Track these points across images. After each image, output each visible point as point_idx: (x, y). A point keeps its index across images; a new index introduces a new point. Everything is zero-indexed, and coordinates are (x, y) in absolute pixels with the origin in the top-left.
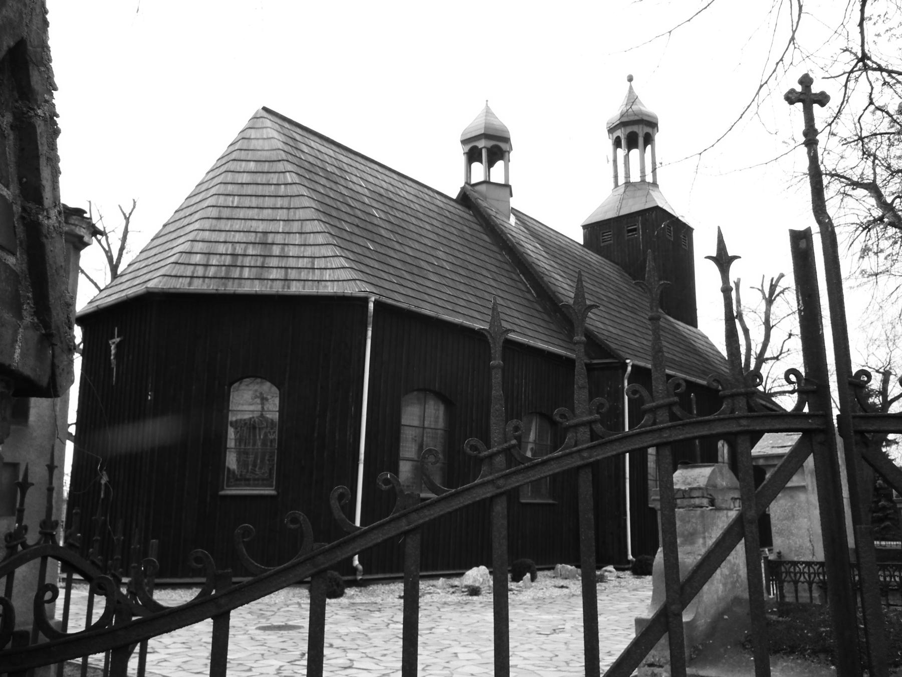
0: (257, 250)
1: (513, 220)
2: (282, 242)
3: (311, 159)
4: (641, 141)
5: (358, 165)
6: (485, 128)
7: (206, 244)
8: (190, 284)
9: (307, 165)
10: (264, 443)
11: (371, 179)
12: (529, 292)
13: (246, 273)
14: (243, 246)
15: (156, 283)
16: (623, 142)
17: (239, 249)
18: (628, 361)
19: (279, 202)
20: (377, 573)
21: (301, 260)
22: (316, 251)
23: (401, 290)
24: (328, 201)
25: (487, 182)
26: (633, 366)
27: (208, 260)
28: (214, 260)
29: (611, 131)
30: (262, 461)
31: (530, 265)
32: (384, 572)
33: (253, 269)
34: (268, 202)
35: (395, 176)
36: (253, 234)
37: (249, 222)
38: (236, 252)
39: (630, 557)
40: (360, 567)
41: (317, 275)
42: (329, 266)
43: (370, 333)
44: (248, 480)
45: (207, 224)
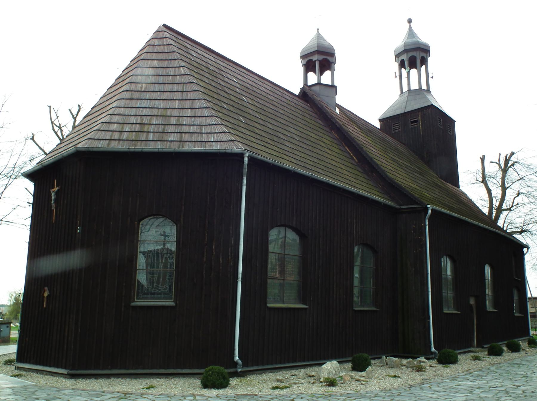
0: (160, 121)
1: (337, 111)
2: (178, 115)
3: (198, 61)
4: (418, 62)
5: (231, 68)
6: (318, 46)
7: (121, 117)
8: (108, 145)
9: (195, 64)
10: (165, 266)
11: (240, 78)
12: (352, 159)
13: (151, 137)
14: (149, 118)
15: (83, 145)
16: (406, 63)
17: (146, 120)
18: (429, 206)
19: (175, 88)
20: (252, 366)
21: (192, 127)
22: (204, 121)
23: (267, 150)
24: (210, 87)
25: (319, 84)
26: (432, 210)
27: (123, 128)
28: (127, 128)
29: (397, 56)
30: (164, 279)
31: (353, 140)
32: (258, 365)
33: (156, 134)
34: (168, 87)
35: (257, 78)
36: (156, 110)
37: (153, 102)
38: (144, 122)
39: (433, 350)
40: (240, 362)
41: (204, 138)
42: (213, 132)
43: (245, 181)
44: (154, 294)
45: (122, 103)
